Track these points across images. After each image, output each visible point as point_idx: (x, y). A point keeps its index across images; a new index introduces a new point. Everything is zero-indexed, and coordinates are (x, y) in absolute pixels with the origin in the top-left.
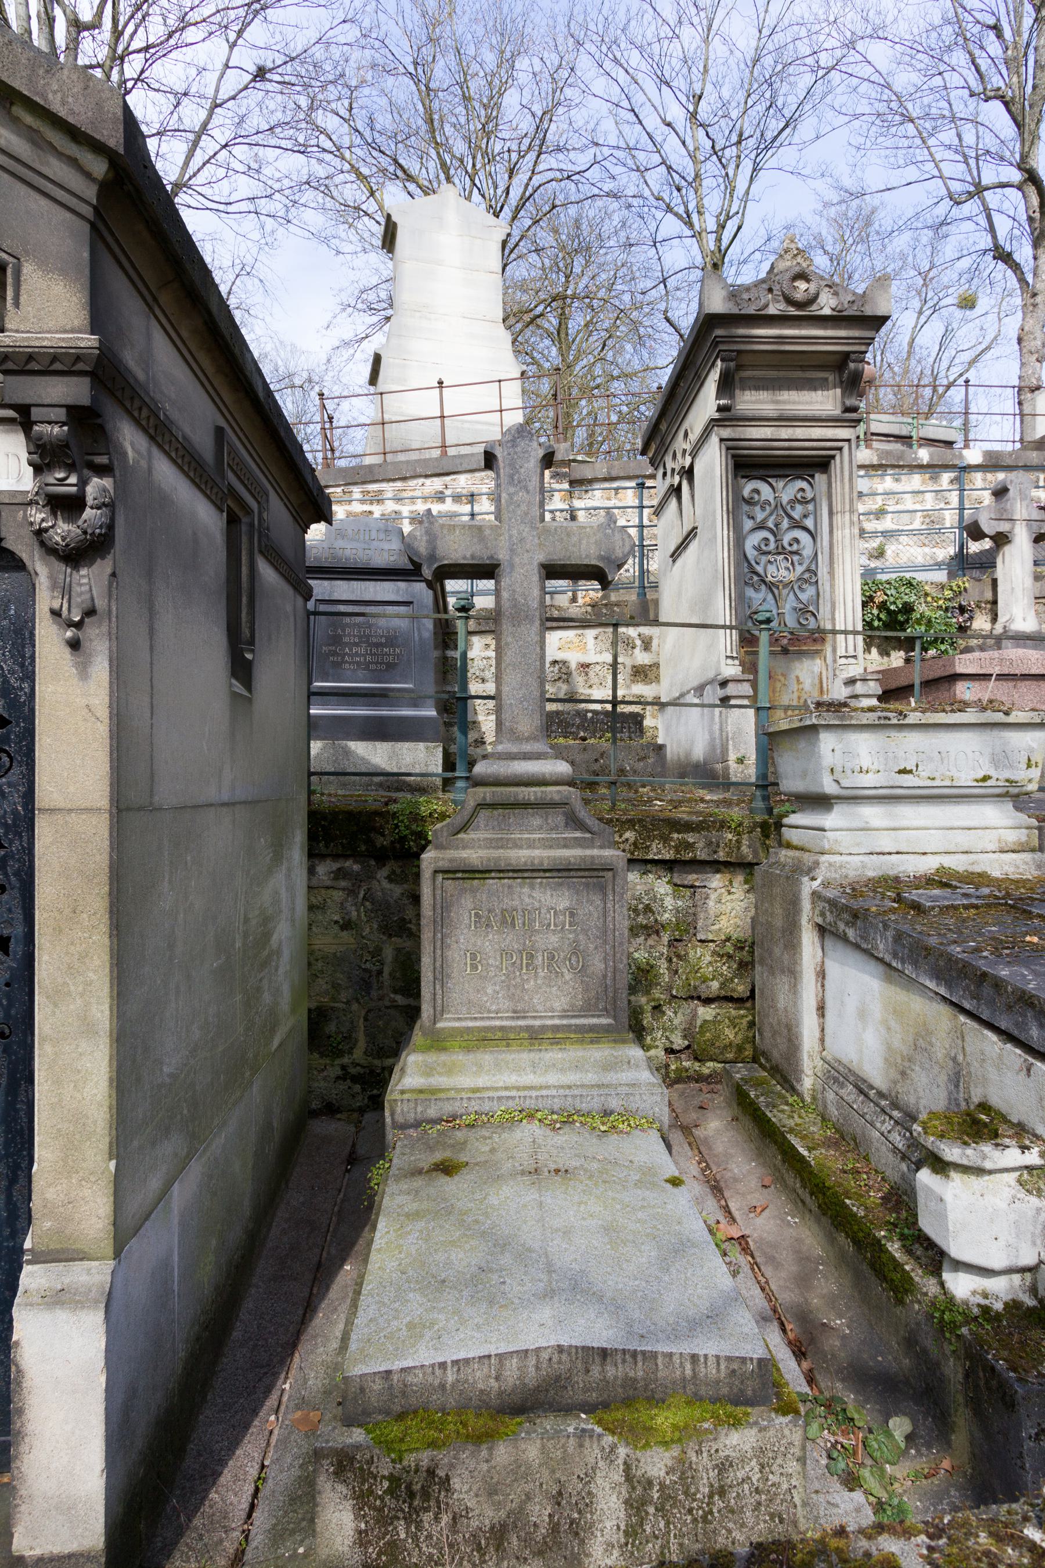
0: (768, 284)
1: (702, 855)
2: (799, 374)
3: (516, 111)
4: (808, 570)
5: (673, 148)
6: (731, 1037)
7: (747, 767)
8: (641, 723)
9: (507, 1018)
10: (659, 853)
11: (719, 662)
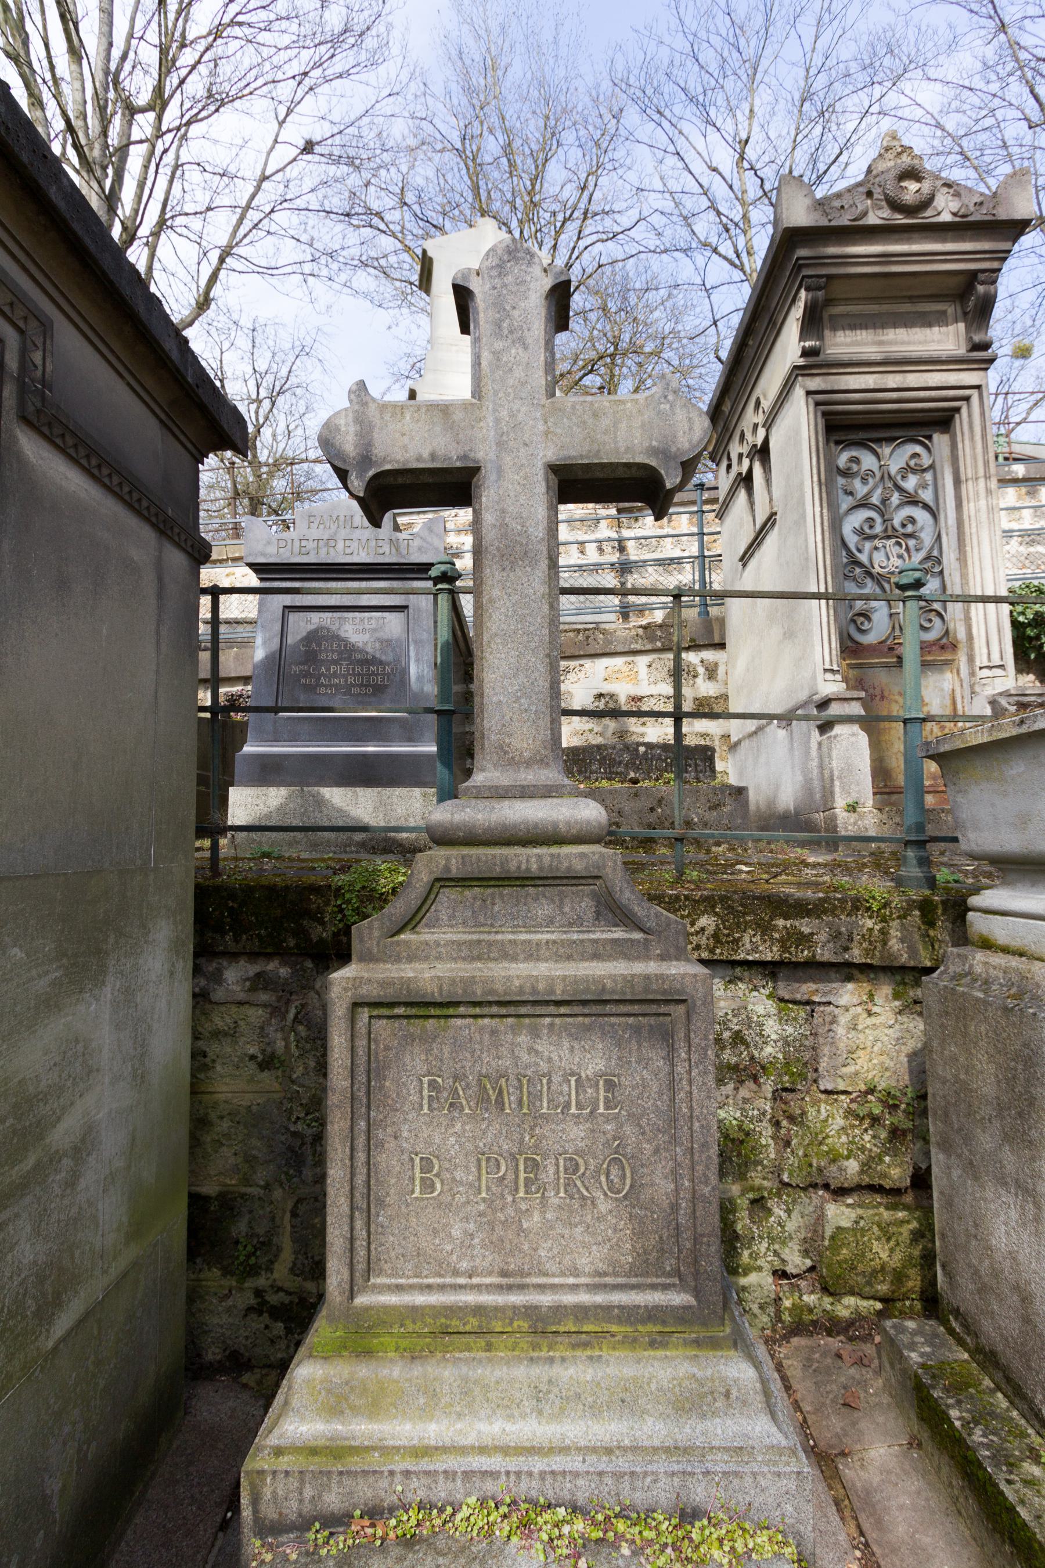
0: (867, 188)
1: (824, 953)
2: (907, 307)
3: (558, 181)
4: (928, 558)
5: (719, 189)
6: (884, 1256)
7: (862, 816)
8: (711, 760)
9: (489, 1288)
10: (755, 950)
11: (814, 677)
